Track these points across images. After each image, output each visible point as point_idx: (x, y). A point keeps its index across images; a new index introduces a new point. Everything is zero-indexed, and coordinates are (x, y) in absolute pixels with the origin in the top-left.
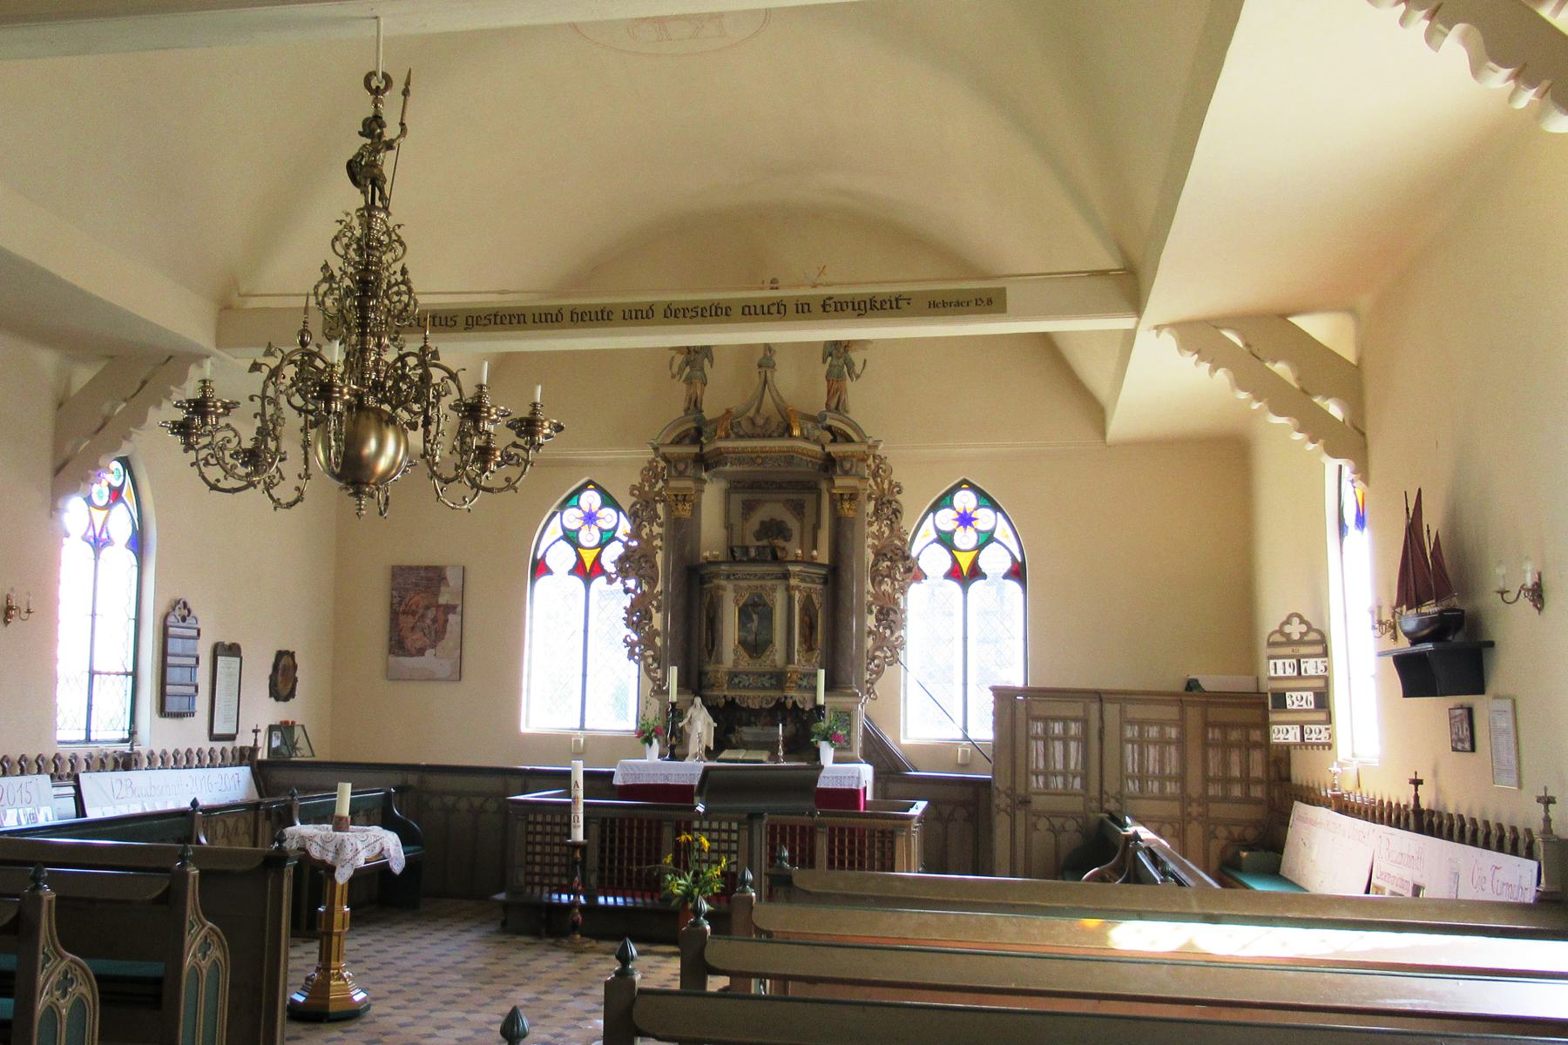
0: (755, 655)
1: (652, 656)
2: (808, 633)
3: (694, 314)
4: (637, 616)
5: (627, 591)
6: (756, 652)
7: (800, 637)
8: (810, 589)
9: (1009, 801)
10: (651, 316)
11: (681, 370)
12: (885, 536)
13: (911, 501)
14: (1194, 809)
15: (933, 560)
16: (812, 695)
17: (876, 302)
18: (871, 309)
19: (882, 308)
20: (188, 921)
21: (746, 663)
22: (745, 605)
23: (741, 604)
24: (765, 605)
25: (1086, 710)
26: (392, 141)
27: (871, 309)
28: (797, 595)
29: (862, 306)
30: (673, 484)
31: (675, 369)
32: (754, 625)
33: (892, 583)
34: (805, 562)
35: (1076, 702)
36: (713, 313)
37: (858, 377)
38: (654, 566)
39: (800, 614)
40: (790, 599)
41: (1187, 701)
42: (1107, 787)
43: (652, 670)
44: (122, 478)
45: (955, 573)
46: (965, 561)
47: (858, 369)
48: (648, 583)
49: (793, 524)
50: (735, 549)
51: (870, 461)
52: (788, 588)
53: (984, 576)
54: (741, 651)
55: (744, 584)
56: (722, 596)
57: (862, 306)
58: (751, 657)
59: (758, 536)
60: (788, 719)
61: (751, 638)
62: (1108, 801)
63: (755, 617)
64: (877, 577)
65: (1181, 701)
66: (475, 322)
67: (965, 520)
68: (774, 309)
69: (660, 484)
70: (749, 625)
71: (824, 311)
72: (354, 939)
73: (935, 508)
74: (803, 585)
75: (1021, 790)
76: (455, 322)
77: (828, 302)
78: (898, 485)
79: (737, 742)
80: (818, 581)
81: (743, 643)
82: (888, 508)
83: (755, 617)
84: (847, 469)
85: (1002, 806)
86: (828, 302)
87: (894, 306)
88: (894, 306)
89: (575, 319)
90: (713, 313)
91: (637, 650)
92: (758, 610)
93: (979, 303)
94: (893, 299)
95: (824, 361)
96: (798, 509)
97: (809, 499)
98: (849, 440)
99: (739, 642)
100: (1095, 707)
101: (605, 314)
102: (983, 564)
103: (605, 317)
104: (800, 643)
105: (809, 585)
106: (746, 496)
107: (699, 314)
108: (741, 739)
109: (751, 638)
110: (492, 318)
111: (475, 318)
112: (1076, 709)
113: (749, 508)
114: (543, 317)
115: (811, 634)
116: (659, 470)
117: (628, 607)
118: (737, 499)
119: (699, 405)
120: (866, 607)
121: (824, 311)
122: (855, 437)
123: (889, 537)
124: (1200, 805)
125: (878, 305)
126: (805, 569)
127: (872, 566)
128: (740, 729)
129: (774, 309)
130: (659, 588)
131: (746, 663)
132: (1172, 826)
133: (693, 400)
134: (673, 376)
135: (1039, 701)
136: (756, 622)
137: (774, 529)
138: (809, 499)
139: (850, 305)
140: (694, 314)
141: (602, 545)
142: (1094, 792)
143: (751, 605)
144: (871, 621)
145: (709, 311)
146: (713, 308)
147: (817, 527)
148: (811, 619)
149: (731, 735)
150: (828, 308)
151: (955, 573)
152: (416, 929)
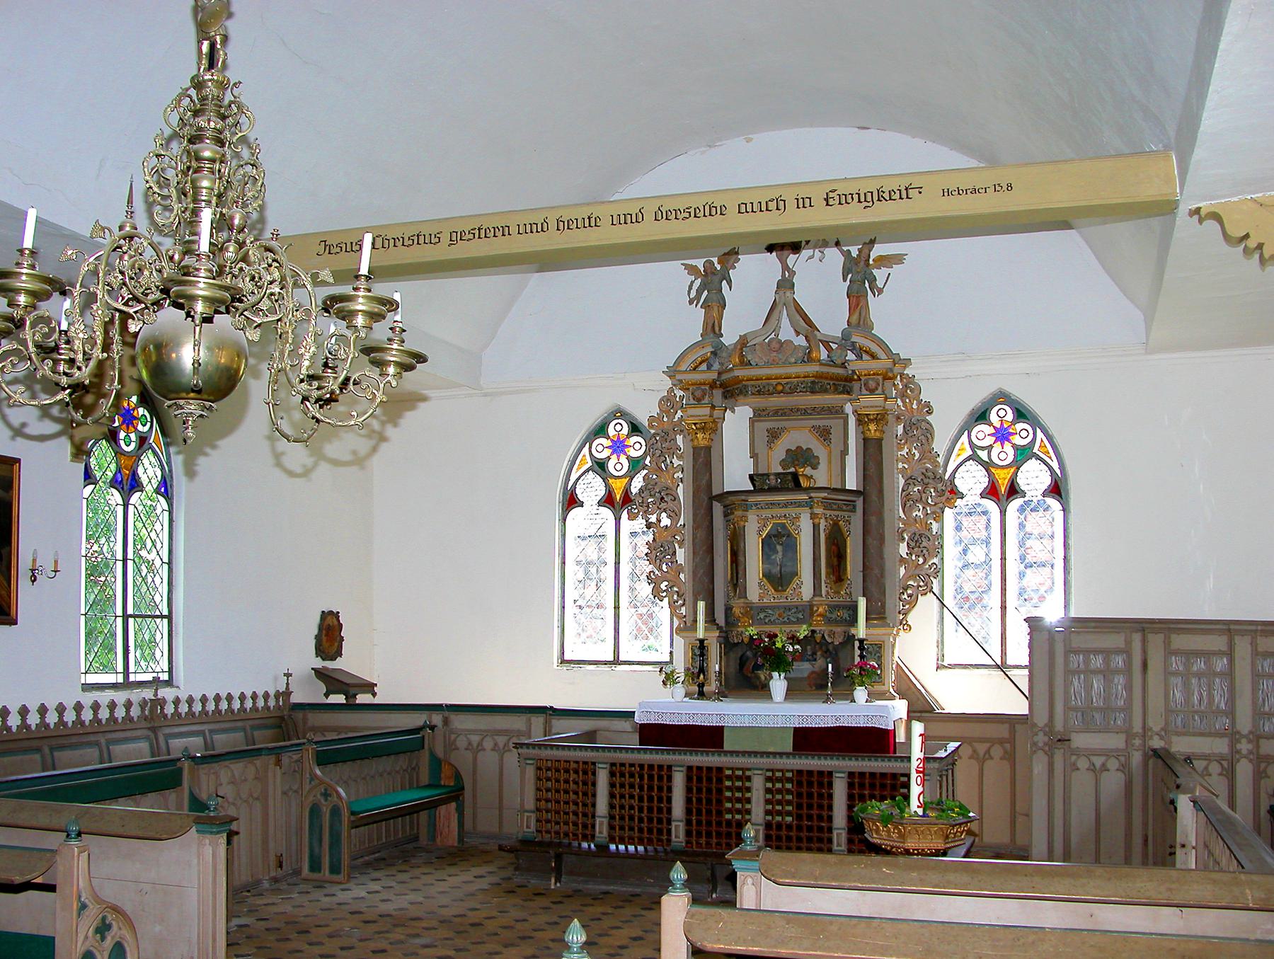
2: (836, 563)
3: (687, 215)
4: (659, 551)
7: (827, 567)
8: (837, 516)
9: (1046, 739)
10: (640, 220)
11: (699, 293)
12: (916, 458)
13: (944, 423)
14: (1244, 746)
15: (971, 480)
17: (884, 192)
18: (879, 200)
19: (890, 199)
20: (713, 672)
21: (772, 598)
22: (769, 535)
24: (789, 535)
25: (1128, 642)
27: (879, 200)
28: (823, 524)
29: (869, 198)
30: (691, 411)
31: (693, 294)
33: (923, 508)
35: (1119, 633)
36: (707, 214)
37: (880, 291)
38: (675, 499)
39: (826, 543)
40: (816, 527)
41: (1236, 630)
42: (1150, 723)
43: (677, 607)
44: (149, 424)
45: (991, 492)
46: (1003, 478)
47: (880, 284)
48: (669, 516)
49: (819, 450)
51: (898, 381)
52: (813, 516)
53: (581, 504)
55: (767, 513)
57: (869, 198)
59: (783, 463)
60: (819, 653)
61: (776, 570)
62: (1151, 738)
63: (779, 548)
64: (908, 501)
65: (1229, 630)
66: (459, 238)
67: (1002, 435)
68: (772, 205)
69: (679, 413)
70: (773, 557)
71: (827, 205)
72: (444, 869)
73: (967, 427)
74: (828, 513)
75: (1059, 725)
76: (439, 238)
77: (831, 195)
78: (928, 405)
80: (844, 508)
81: (767, 575)
82: (920, 430)
85: (1041, 744)
86: (831, 195)
87: (904, 196)
88: (904, 196)
89: (561, 228)
90: (707, 214)
91: (663, 586)
92: (780, 540)
93: (998, 188)
94: (903, 189)
95: (845, 280)
96: (824, 434)
97: (834, 424)
98: (873, 356)
100: (1137, 638)
101: (593, 220)
102: (1021, 481)
103: (593, 224)
104: (828, 574)
105: (836, 513)
106: (769, 425)
107: (693, 215)
109: (776, 570)
110: (477, 232)
111: (459, 234)
112: (1116, 641)
113: (774, 435)
114: (528, 227)
115: (839, 565)
116: (678, 399)
118: (763, 426)
119: (717, 329)
121: (827, 205)
123: (920, 460)
124: (1250, 741)
125: (886, 196)
126: (830, 496)
127: (903, 490)
129: (772, 205)
130: (681, 522)
131: (772, 598)
132: (1221, 764)
133: (711, 325)
134: (691, 302)
135: (1078, 632)
136: (780, 554)
137: (801, 457)
138: (834, 424)
139: (856, 197)
140: (687, 215)
141: (631, 475)
142: (1137, 727)
143: (774, 536)
144: (903, 549)
145: (702, 211)
146: (707, 208)
147: (845, 452)
148: (839, 549)
150: (831, 202)
151: (991, 492)
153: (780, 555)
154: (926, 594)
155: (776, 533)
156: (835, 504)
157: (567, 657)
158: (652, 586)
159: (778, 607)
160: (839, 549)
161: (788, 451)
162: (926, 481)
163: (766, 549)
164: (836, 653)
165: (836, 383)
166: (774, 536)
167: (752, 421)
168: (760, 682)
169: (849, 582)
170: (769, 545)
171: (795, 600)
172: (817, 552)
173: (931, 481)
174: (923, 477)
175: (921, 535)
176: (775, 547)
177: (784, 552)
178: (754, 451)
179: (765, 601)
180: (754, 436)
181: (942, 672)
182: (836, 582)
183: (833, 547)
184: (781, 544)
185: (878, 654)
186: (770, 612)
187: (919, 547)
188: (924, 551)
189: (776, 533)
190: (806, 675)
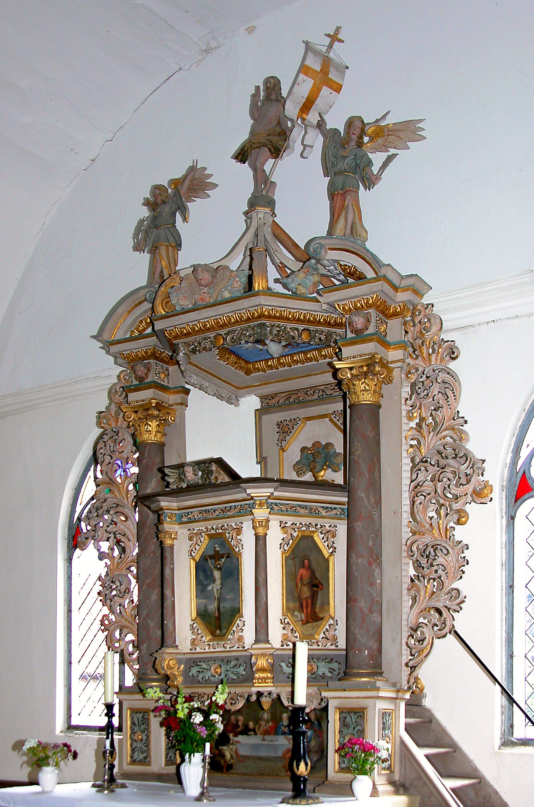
0: (218, 632)
1: (133, 641)
5: (102, 556)
6: (220, 629)
8: (308, 526)
16: (152, 715)
22: (204, 558)
23: (197, 558)
26: (411, 448)
32: (215, 587)
34: (271, 480)
50: (166, 471)
54: (201, 629)
56: (172, 547)
58: (213, 634)
61: (212, 607)
63: (217, 574)
70: (210, 588)
79: (232, 757)
80: (323, 513)
83: (217, 574)
84: (359, 326)
98: (360, 278)
99: (197, 614)
105: (306, 520)
108: (236, 752)
109: (212, 607)
115: (314, 597)
117: (103, 575)
120: (404, 548)
122: (370, 274)
128: (236, 739)
136: (218, 582)
143: (211, 557)
149: (224, 748)
152: (336, 781)
153: (217, 585)
154: (444, 636)
155: (211, 553)
156: (306, 507)
157: (74, 722)
158: (106, 633)
159: (214, 660)
160: (313, 573)
161: (303, 450)
162: (443, 462)
163: (202, 577)
164: (320, 724)
165: (312, 328)
166: (211, 557)
167: (259, 413)
168: (225, 762)
169: (331, 622)
170: (205, 571)
171: (235, 648)
172: (261, 580)
173: (451, 461)
174: (438, 457)
175: (435, 547)
176: (212, 573)
177: (223, 579)
178: (261, 454)
179: (198, 650)
180: (261, 435)
181: (508, 751)
182: (305, 622)
183: (302, 571)
184: (220, 569)
185: (359, 727)
186: (204, 666)
187: (432, 565)
188: (440, 571)
189: (213, 553)
190: (280, 754)
